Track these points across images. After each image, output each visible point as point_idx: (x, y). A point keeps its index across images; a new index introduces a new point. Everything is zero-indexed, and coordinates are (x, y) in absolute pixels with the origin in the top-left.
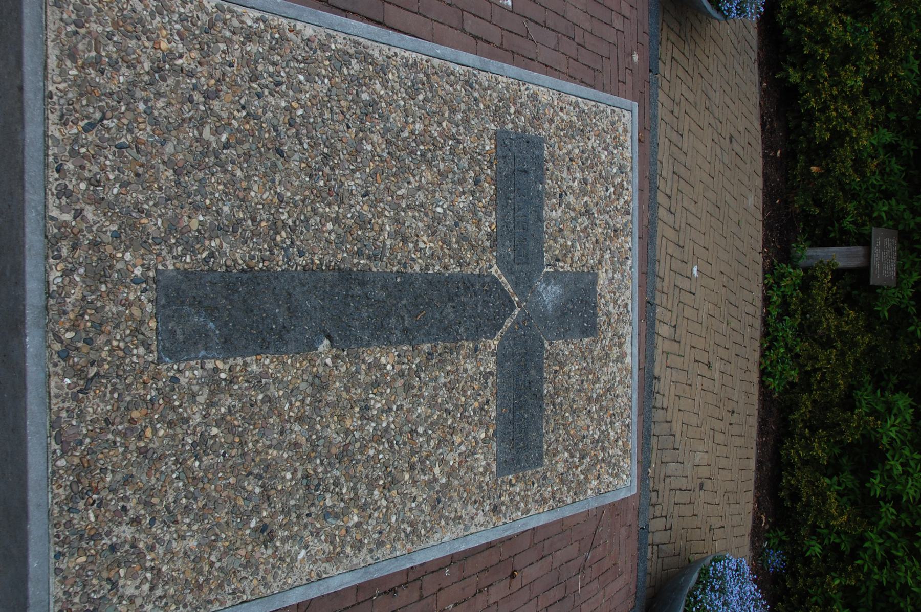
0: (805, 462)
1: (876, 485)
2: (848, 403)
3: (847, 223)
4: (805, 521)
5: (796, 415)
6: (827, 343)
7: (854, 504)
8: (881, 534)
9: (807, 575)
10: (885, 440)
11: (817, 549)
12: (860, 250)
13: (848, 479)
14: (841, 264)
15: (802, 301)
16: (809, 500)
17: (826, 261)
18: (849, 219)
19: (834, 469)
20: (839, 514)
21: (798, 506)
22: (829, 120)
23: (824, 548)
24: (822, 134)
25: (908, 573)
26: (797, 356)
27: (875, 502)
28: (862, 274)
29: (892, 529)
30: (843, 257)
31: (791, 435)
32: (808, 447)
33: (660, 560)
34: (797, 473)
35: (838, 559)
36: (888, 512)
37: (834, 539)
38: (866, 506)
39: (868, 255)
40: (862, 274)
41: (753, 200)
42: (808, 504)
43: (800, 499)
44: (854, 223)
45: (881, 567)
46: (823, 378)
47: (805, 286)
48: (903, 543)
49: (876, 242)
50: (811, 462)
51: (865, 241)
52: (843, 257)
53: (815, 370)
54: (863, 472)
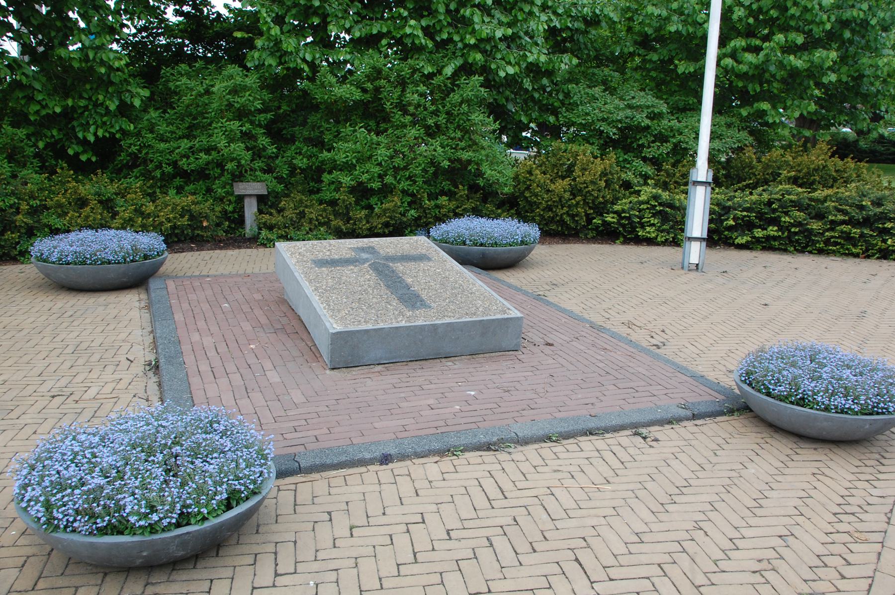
0: (368, 222)
1: (376, 185)
2: (333, 203)
3: (230, 208)
4: (400, 219)
5: (343, 227)
6: (302, 215)
7: (385, 197)
8: (399, 183)
9: (426, 217)
10: (353, 183)
11: (412, 212)
12: (247, 201)
13: (373, 200)
14: (255, 210)
15: (279, 229)
16: (389, 217)
17: (255, 218)
18: (227, 208)
19: (370, 207)
20: (395, 202)
21: (392, 222)
22: (175, 218)
23: (412, 209)
24: (185, 221)
25: (886, 131)
26: (310, 229)
27: (385, 185)
28: (261, 199)
29: (395, 178)
30: (251, 209)
31: (354, 230)
32: (360, 220)
33: (467, 524)
34: (375, 224)
35: (415, 202)
36: (389, 179)
37: (406, 204)
38: (386, 191)
39: (250, 196)
40: (261, 199)
41: (235, 252)
42: (390, 217)
43: (388, 222)
44: (229, 205)
45: (415, 182)
46: (321, 215)
47: (271, 228)
48: (401, 173)
49: (242, 192)
50: (367, 217)
51: (241, 199)
52: (251, 209)
53: (317, 220)
54: (371, 192)
